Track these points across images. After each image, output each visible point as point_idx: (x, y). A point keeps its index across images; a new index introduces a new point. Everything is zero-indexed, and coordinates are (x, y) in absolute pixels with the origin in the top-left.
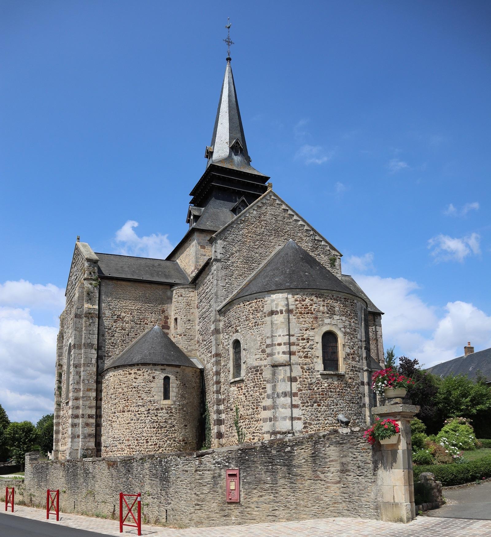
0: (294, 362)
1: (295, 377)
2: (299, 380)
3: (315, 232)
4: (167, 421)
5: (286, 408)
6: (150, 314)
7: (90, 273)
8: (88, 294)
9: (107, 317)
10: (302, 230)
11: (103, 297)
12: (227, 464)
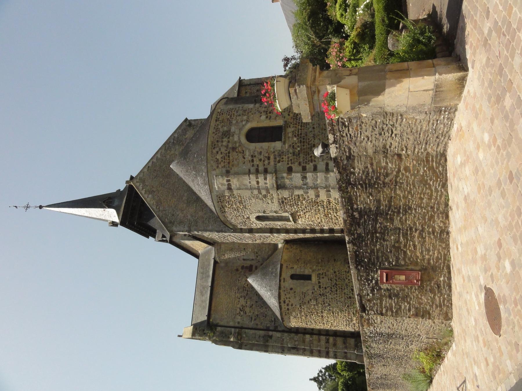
2: (290, 165)
12: (374, 282)
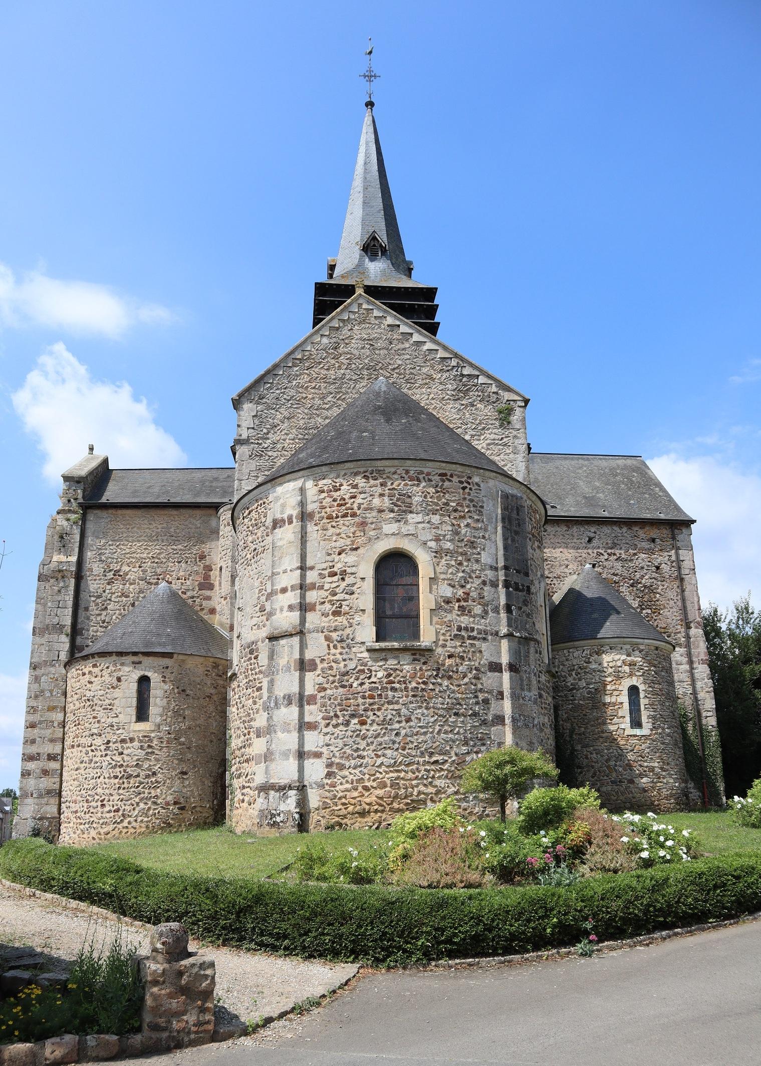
0: (311, 627)
1: (313, 660)
2: (320, 666)
3: (462, 361)
4: (140, 763)
5: (289, 732)
6: (176, 564)
7: (69, 501)
8: (62, 537)
9: (95, 576)
10: (432, 359)
11: (89, 540)
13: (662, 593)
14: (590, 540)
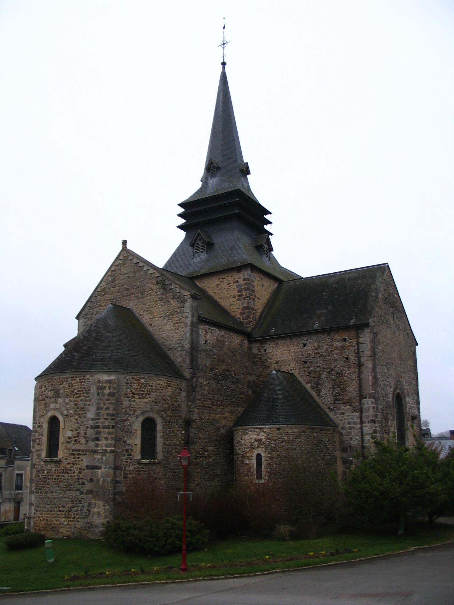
13: (348, 376)
14: (305, 345)
